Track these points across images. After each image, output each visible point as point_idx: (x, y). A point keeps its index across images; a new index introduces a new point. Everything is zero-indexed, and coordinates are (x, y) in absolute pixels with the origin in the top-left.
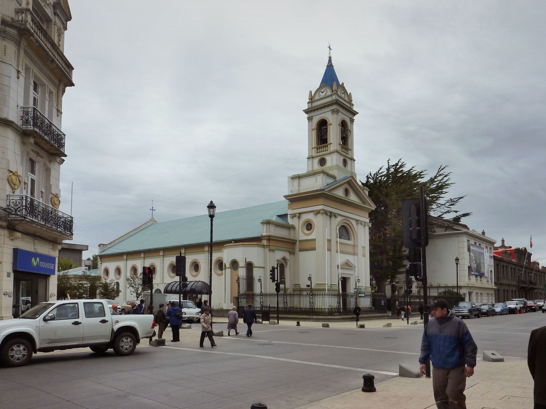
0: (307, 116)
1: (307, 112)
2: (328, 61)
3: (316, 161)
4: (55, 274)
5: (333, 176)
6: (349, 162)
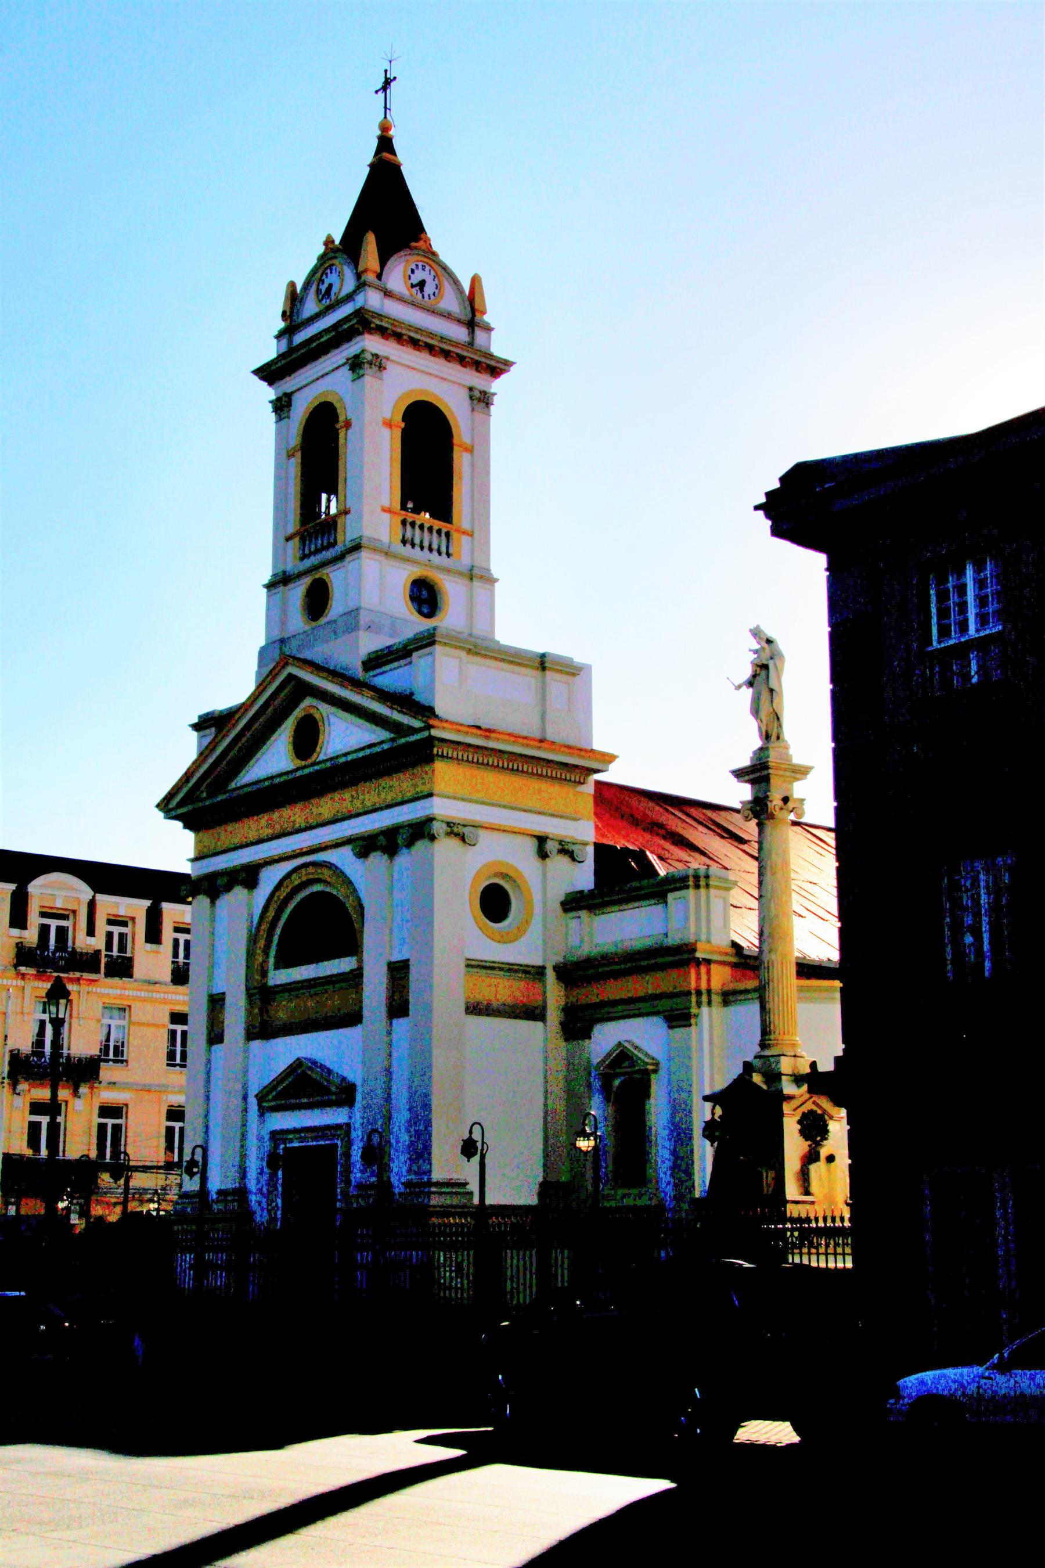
0: (268, 393)
1: (268, 373)
2: (376, 141)
3: (298, 592)
4: (4, 1159)
5: (387, 655)
6: (452, 589)
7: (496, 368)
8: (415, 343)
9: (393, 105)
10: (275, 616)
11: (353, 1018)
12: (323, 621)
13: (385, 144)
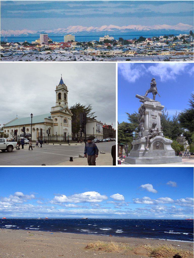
0: (55, 92)
1: (56, 91)
3: (58, 103)
7: (68, 91)
13: (62, 78)
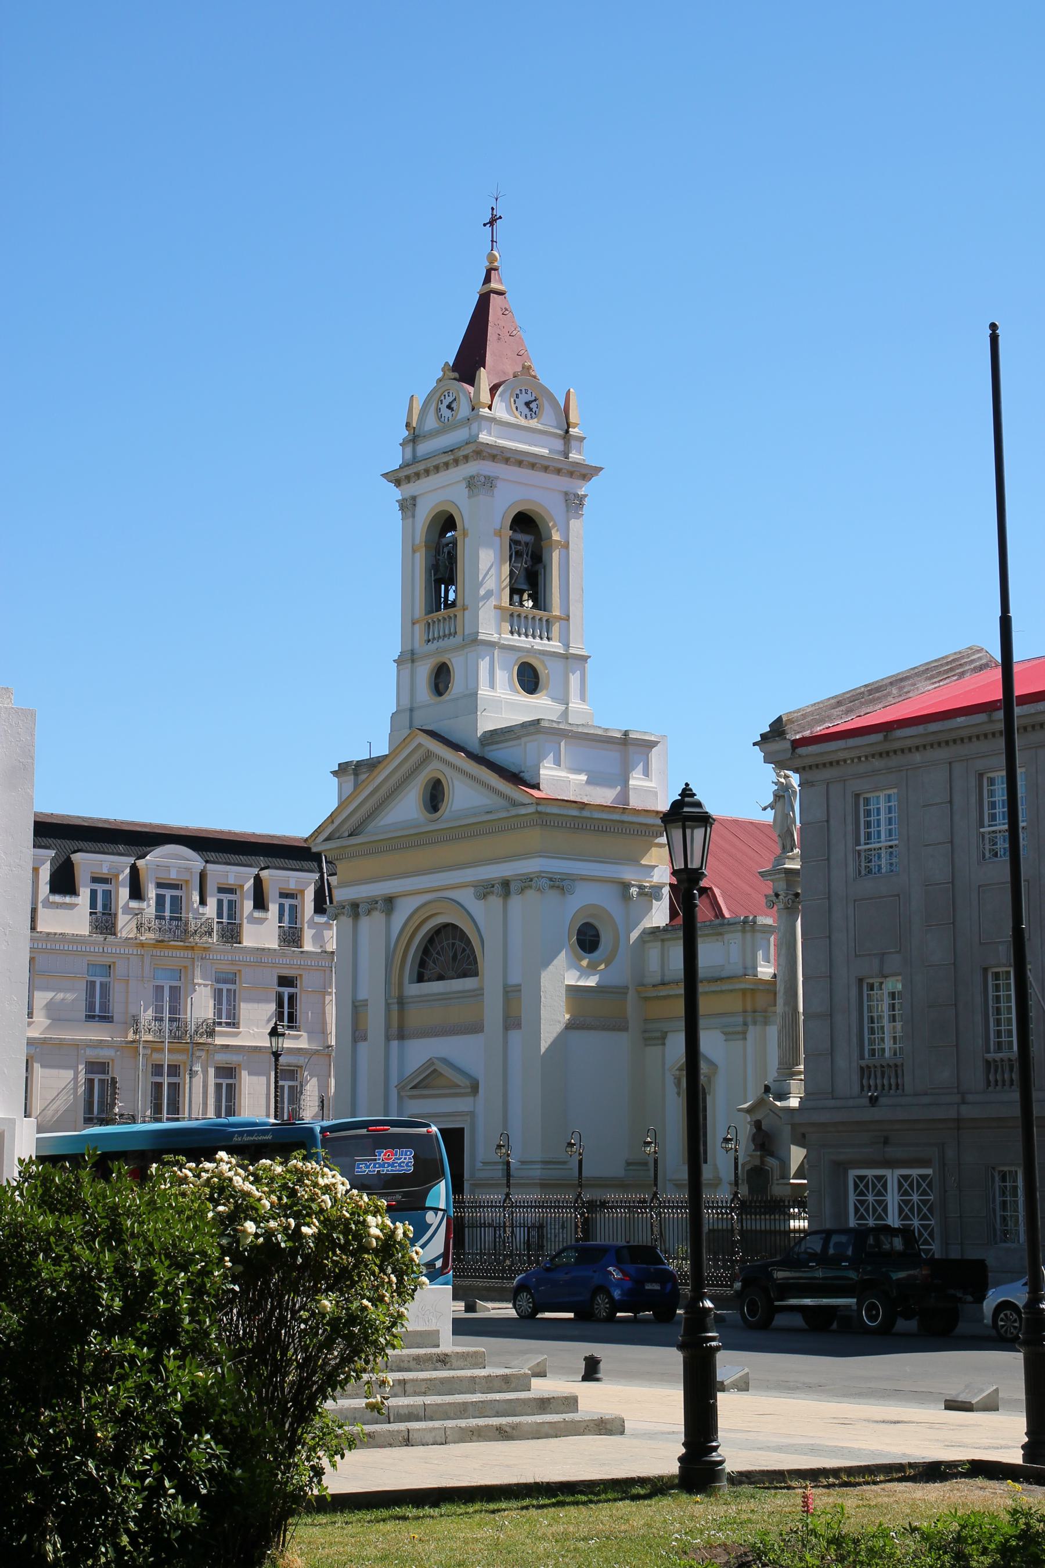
0: (396, 494)
1: (397, 479)
3: (424, 671)
7: (586, 473)
8: (520, 463)
9: (498, 237)
10: (406, 687)
11: (476, 1028)
12: (445, 697)
